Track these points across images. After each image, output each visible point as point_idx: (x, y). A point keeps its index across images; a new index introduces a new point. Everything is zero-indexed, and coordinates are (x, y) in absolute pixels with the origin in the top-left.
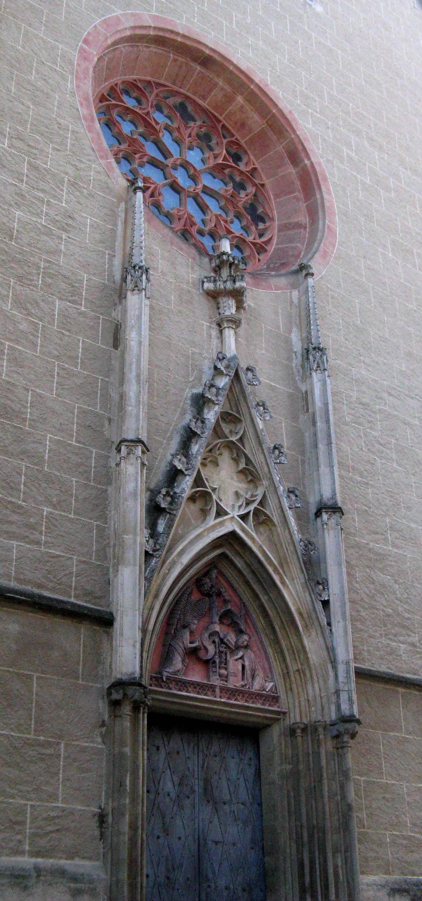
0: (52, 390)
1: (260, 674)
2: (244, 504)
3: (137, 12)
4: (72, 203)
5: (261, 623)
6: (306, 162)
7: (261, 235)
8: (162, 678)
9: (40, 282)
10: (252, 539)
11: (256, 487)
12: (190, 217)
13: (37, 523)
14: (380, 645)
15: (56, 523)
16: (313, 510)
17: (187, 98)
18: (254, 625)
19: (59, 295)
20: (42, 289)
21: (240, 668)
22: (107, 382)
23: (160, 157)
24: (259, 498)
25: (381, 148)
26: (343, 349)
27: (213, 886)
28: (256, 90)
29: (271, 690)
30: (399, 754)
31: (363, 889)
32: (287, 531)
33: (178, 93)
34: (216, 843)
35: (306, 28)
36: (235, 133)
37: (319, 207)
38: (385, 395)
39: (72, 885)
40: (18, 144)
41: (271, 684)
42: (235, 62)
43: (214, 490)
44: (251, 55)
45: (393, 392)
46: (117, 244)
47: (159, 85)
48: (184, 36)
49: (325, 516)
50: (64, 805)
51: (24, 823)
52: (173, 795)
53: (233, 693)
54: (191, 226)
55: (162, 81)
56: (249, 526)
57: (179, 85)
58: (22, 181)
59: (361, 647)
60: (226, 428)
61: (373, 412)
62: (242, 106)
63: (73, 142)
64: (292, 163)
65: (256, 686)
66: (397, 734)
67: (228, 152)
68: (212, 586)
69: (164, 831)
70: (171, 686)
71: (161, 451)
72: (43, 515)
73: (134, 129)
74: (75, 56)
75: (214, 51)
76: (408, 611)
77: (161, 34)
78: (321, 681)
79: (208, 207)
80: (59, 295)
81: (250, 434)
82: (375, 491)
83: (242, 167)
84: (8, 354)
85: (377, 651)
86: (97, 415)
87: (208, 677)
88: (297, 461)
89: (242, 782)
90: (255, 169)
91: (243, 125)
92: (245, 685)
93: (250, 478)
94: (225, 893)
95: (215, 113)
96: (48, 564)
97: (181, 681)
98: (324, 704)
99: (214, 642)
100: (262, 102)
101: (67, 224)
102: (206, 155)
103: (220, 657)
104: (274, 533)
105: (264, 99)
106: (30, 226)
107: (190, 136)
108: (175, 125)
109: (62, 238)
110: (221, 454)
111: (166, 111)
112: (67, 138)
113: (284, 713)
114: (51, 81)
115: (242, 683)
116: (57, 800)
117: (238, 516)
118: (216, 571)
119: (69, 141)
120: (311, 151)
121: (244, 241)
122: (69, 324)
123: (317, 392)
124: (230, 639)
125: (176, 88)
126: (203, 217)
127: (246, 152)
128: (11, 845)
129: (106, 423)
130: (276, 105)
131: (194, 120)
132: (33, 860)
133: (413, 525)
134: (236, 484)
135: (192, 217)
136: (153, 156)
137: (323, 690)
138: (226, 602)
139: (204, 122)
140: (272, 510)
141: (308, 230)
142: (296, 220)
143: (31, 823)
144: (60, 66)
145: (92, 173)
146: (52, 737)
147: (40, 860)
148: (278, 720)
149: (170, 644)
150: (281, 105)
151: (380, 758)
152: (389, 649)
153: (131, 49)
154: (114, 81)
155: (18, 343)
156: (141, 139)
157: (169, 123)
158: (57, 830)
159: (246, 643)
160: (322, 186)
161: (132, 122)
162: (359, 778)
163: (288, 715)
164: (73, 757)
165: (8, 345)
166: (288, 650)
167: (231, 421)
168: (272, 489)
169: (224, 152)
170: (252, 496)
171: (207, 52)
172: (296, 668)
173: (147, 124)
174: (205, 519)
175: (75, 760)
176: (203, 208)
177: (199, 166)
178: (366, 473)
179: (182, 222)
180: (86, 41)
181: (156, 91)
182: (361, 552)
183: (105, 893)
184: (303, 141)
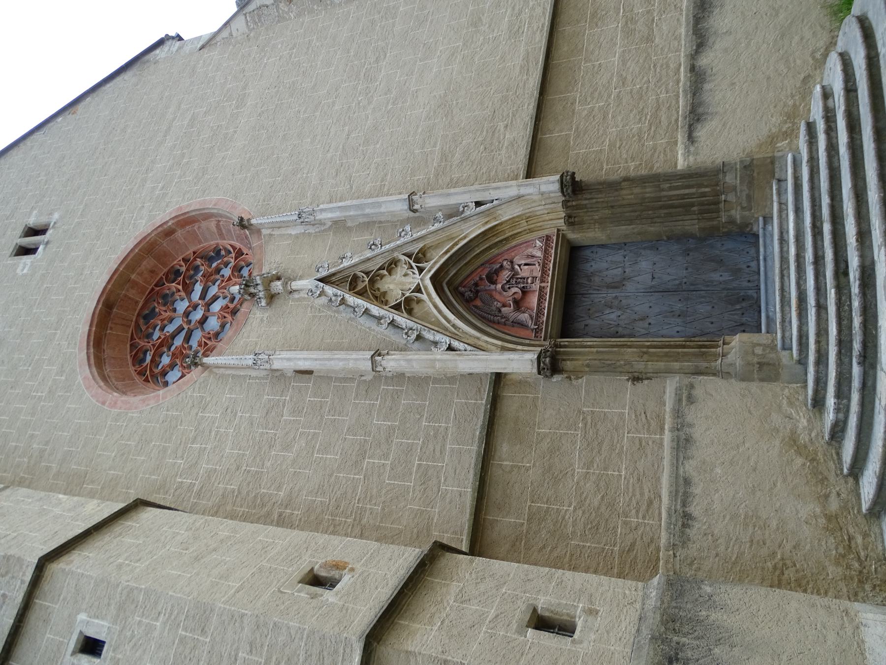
0: (344, 420)
1: (530, 251)
2: (412, 270)
3: (77, 363)
4: (217, 409)
5: (495, 251)
6: (170, 224)
7: (230, 252)
8: (536, 329)
9: (272, 431)
10: (435, 263)
11: (399, 260)
12: (222, 309)
13: (434, 430)
14: (506, 156)
15: (433, 416)
16: (412, 214)
17: (138, 315)
18: (495, 257)
19: (280, 417)
20: (277, 430)
21: (526, 267)
22: (336, 378)
23: (183, 334)
24: (407, 259)
25: (153, 162)
26: (299, 191)
27: (685, 280)
28: (123, 266)
29: (541, 242)
30: (586, 136)
31: (688, 165)
32: (428, 236)
33: (137, 322)
34: (653, 278)
35: (72, 226)
36: (159, 277)
37: (201, 212)
38: (329, 155)
39: (684, 403)
40: (180, 453)
41: (537, 242)
42: (104, 284)
43: (403, 295)
44: (98, 271)
45: (327, 148)
46: (242, 374)
47: (132, 338)
48: (91, 326)
49: (416, 207)
50: (627, 408)
51: (640, 440)
52: (619, 313)
53: (544, 271)
54: (229, 308)
55: (130, 335)
56: (427, 266)
57: (130, 322)
58: (205, 448)
59: (509, 171)
60: (360, 286)
61: (342, 166)
62: (138, 274)
63: (175, 410)
64: (174, 233)
65: (539, 254)
66: (572, 138)
67: (173, 282)
68: (471, 291)
69: (645, 319)
70: (541, 321)
71: (379, 336)
72: (428, 426)
73: (166, 354)
74: (115, 411)
75: (99, 301)
76: (482, 132)
77: (92, 343)
78: (533, 205)
79: (214, 295)
80: (280, 417)
81: (363, 267)
82: (397, 162)
83: (183, 269)
84: (322, 454)
85: (511, 157)
86: (358, 386)
87: (534, 291)
88: (379, 227)
89: (609, 259)
90: (183, 259)
91: (152, 272)
92: (539, 263)
93: (393, 266)
94: (690, 270)
95: (147, 293)
96: (461, 421)
97: (537, 314)
98: (550, 202)
99: (509, 288)
100: (131, 260)
101: (232, 413)
102: (178, 297)
103: (519, 283)
104: (430, 245)
105: (129, 259)
106: (235, 441)
107: (166, 311)
108: (159, 322)
109: (241, 416)
110: (378, 289)
111: (151, 330)
112: (172, 415)
113: (558, 230)
114: (134, 429)
115: (537, 265)
116: (623, 414)
117: (420, 275)
118: (460, 288)
119: (174, 413)
120: (161, 221)
121: (234, 266)
122: (299, 408)
123: (330, 215)
124: (506, 276)
125: (133, 323)
126: (221, 297)
127: (173, 267)
128: (656, 448)
129: (363, 378)
130: (132, 250)
131: (154, 308)
132: (667, 432)
133: (420, 130)
134: (399, 275)
135: (222, 307)
136: (183, 338)
137: (540, 203)
138: (481, 279)
139: (155, 301)
140: (415, 248)
141: (220, 219)
142: (214, 228)
143: (640, 433)
144: (123, 422)
145: (195, 395)
146: (579, 417)
147: (666, 427)
148: (563, 234)
149: (512, 322)
150: (131, 246)
151: (590, 152)
152: (509, 147)
153: (107, 364)
154: (134, 374)
155: (314, 447)
156: (173, 348)
157: (158, 328)
158: (645, 413)
159: (509, 263)
160: (186, 211)
161: (161, 356)
162: (604, 170)
163: (559, 228)
164: (592, 401)
165: (317, 454)
166: (513, 231)
167: (356, 282)
168: (399, 249)
169: (174, 284)
170: (406, 264)
171: (100, 306)
172: (526, 224)
173: (161, 345)
174: (423, 300)
175: (595, 400)
176: (215, 298)
177: (186, 304)
178: (385, 171)
179: (226, 315)
180: (104, 403)
181: (137, 340)
182: (441, 173)
183: (690, 378)
184: (155, 227)
